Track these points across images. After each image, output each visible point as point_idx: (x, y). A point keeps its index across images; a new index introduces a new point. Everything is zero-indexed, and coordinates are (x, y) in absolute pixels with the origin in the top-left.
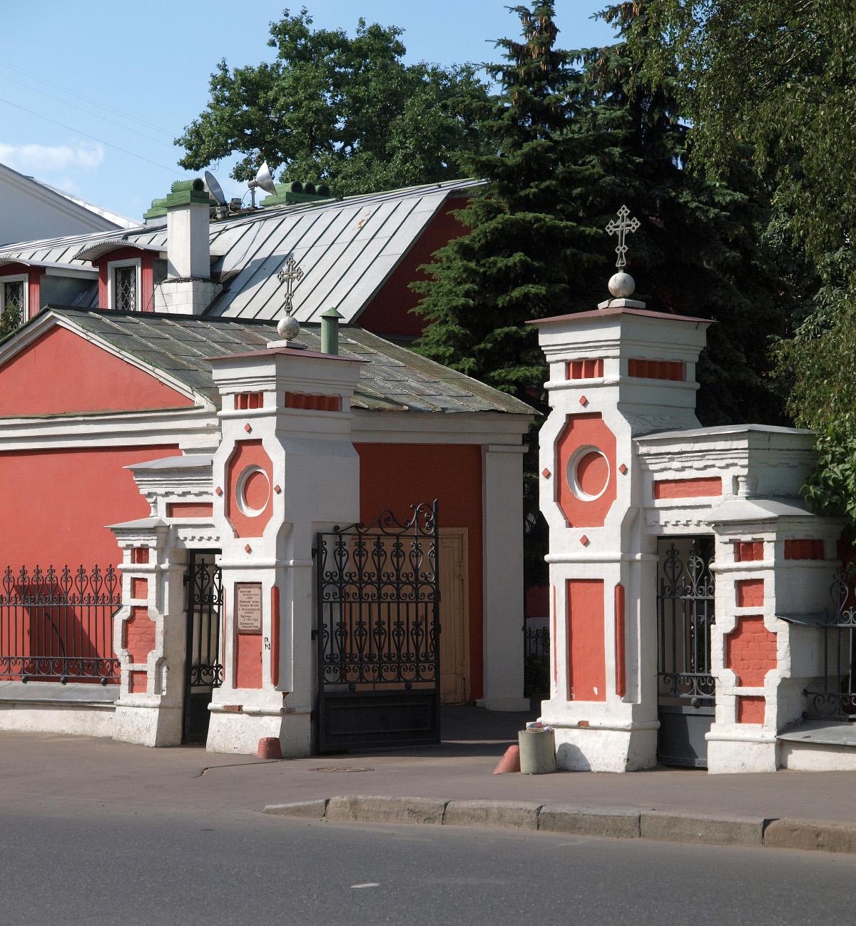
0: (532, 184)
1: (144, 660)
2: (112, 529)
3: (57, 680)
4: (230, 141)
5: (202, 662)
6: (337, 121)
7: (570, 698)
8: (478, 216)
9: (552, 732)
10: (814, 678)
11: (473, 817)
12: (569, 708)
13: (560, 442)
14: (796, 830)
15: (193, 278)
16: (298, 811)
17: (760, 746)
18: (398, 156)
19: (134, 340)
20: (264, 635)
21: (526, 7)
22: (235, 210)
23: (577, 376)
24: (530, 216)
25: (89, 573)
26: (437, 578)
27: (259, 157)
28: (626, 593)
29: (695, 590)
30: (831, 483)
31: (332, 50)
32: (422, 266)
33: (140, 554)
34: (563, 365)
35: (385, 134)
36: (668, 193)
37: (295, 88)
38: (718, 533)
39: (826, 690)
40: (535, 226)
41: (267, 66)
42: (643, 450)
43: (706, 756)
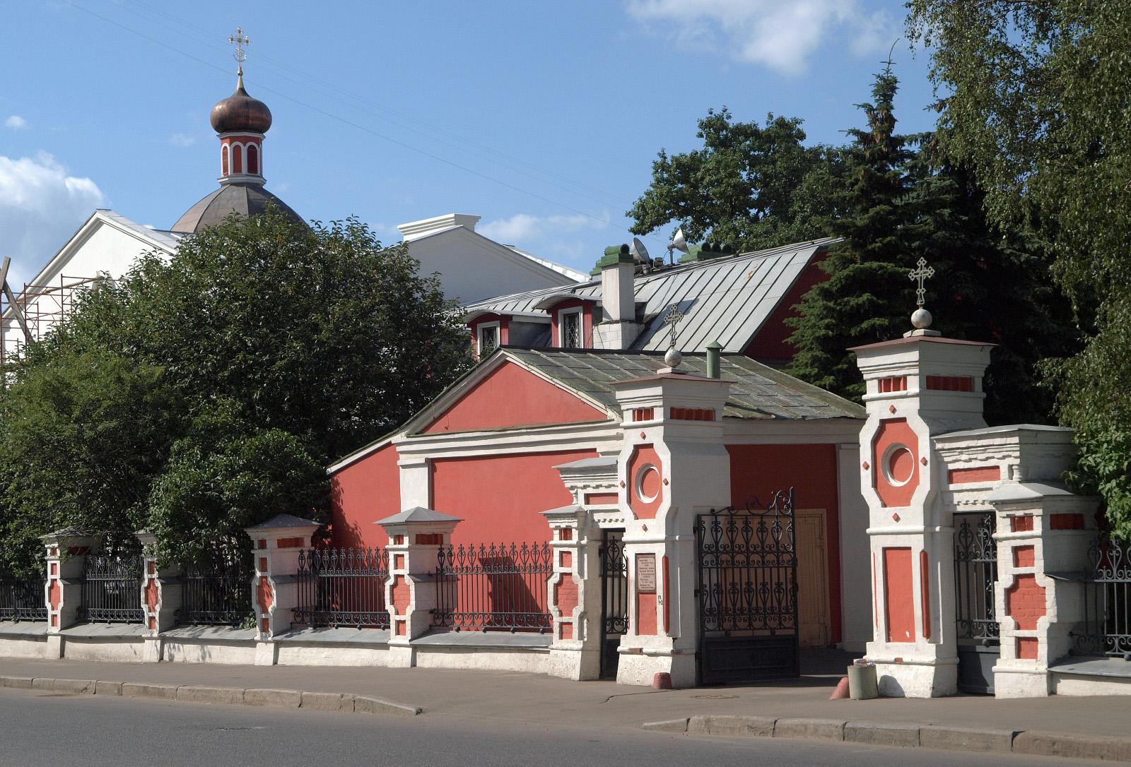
0: (877, 240)
1: (570, 614)
2: (545, 515)
3: (508, 630)
4: (667, 212)
5: (615, 615)
6: (752, 193)
7: (888, 640)
8: (836, 266)
9: (874, 667)
10: (1078, 623)
11: (795, 731)
12: (887, 648)
13: (875, 441)
14: (1036, 740)
15: (622, 320)
16: (666, 727)
17: (1035, 676)
18: (799, 218)
19: (564, 371)
20: (658, 594)
21: (870, 104)
22: (657, 267)
23: (888, 390)
24: (875, 265)
25: (530, 548)
26: (794, 549)
27: (692, 223)
28: (929, 558)
29: (983, 554)
30: (1086, 469)
31: (747, 138)
32: (794, 306)
33: (566, 533)
34: (876, 382)
35: (789, 202)
36: (988, 243)
37: (718, 169)
38: (998, 510)
39: (1087, 632)
40: (879, 273)
41: (697, 153)
42: (939, 446)
43: (994, 686)
